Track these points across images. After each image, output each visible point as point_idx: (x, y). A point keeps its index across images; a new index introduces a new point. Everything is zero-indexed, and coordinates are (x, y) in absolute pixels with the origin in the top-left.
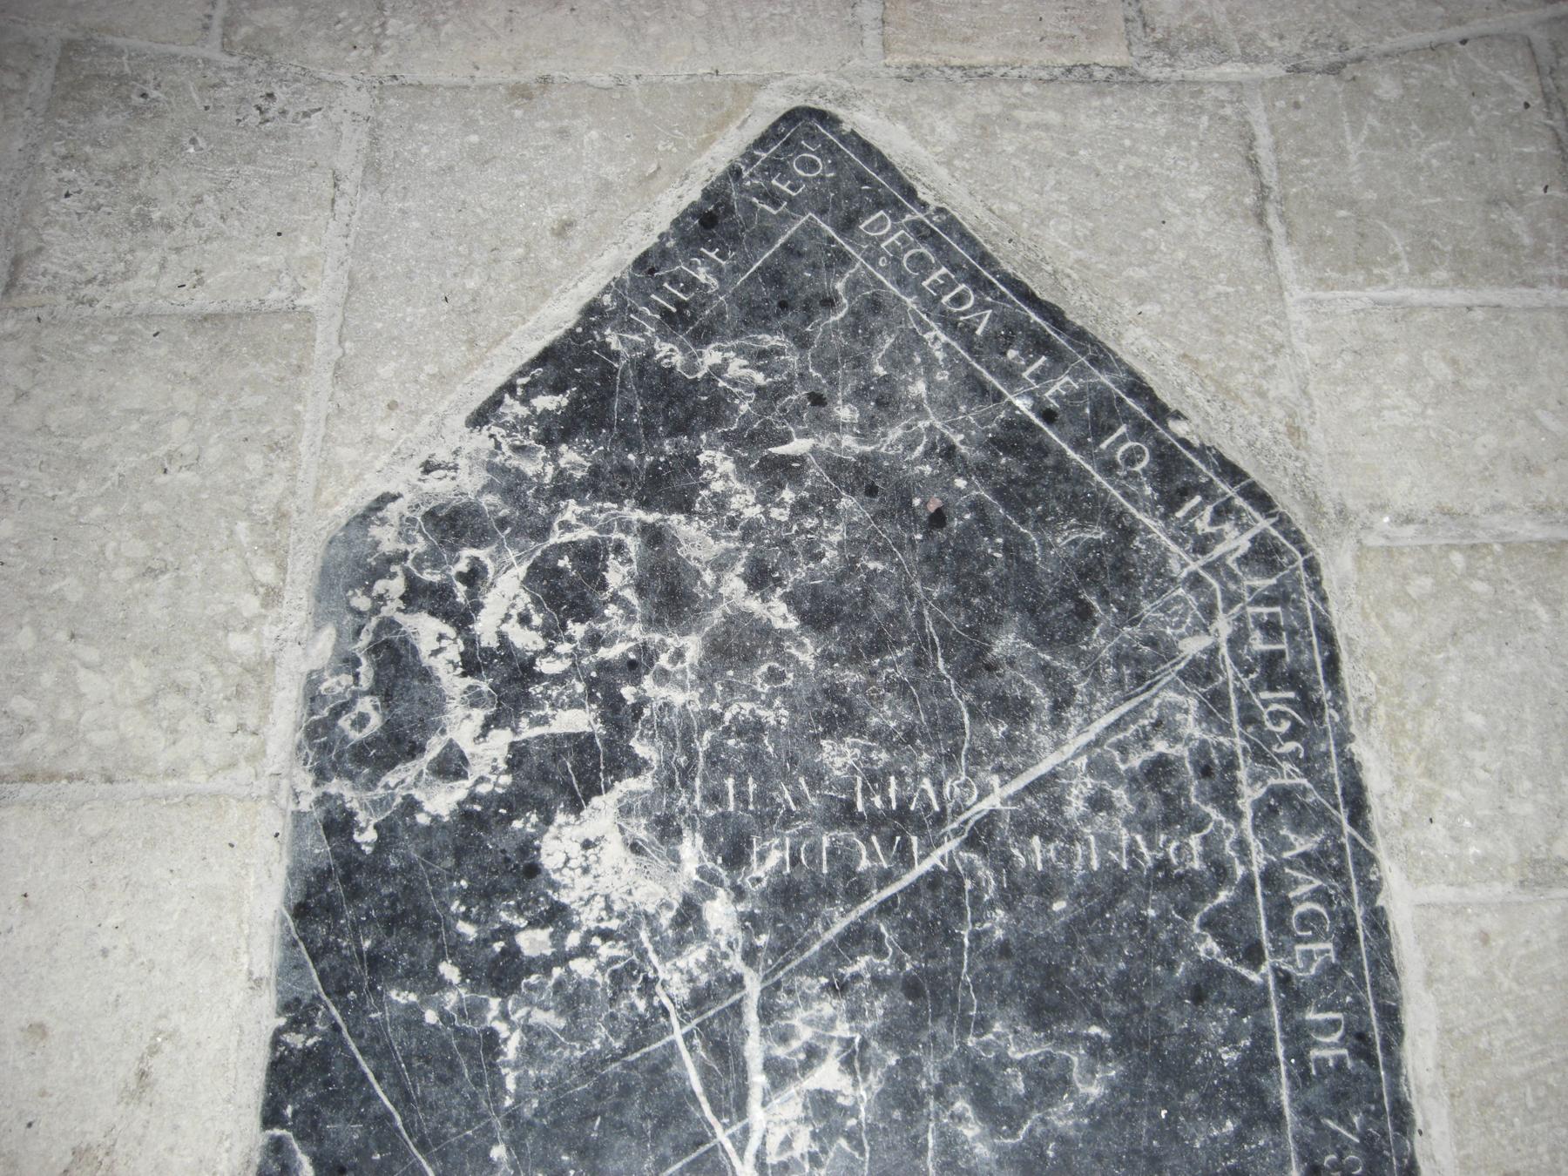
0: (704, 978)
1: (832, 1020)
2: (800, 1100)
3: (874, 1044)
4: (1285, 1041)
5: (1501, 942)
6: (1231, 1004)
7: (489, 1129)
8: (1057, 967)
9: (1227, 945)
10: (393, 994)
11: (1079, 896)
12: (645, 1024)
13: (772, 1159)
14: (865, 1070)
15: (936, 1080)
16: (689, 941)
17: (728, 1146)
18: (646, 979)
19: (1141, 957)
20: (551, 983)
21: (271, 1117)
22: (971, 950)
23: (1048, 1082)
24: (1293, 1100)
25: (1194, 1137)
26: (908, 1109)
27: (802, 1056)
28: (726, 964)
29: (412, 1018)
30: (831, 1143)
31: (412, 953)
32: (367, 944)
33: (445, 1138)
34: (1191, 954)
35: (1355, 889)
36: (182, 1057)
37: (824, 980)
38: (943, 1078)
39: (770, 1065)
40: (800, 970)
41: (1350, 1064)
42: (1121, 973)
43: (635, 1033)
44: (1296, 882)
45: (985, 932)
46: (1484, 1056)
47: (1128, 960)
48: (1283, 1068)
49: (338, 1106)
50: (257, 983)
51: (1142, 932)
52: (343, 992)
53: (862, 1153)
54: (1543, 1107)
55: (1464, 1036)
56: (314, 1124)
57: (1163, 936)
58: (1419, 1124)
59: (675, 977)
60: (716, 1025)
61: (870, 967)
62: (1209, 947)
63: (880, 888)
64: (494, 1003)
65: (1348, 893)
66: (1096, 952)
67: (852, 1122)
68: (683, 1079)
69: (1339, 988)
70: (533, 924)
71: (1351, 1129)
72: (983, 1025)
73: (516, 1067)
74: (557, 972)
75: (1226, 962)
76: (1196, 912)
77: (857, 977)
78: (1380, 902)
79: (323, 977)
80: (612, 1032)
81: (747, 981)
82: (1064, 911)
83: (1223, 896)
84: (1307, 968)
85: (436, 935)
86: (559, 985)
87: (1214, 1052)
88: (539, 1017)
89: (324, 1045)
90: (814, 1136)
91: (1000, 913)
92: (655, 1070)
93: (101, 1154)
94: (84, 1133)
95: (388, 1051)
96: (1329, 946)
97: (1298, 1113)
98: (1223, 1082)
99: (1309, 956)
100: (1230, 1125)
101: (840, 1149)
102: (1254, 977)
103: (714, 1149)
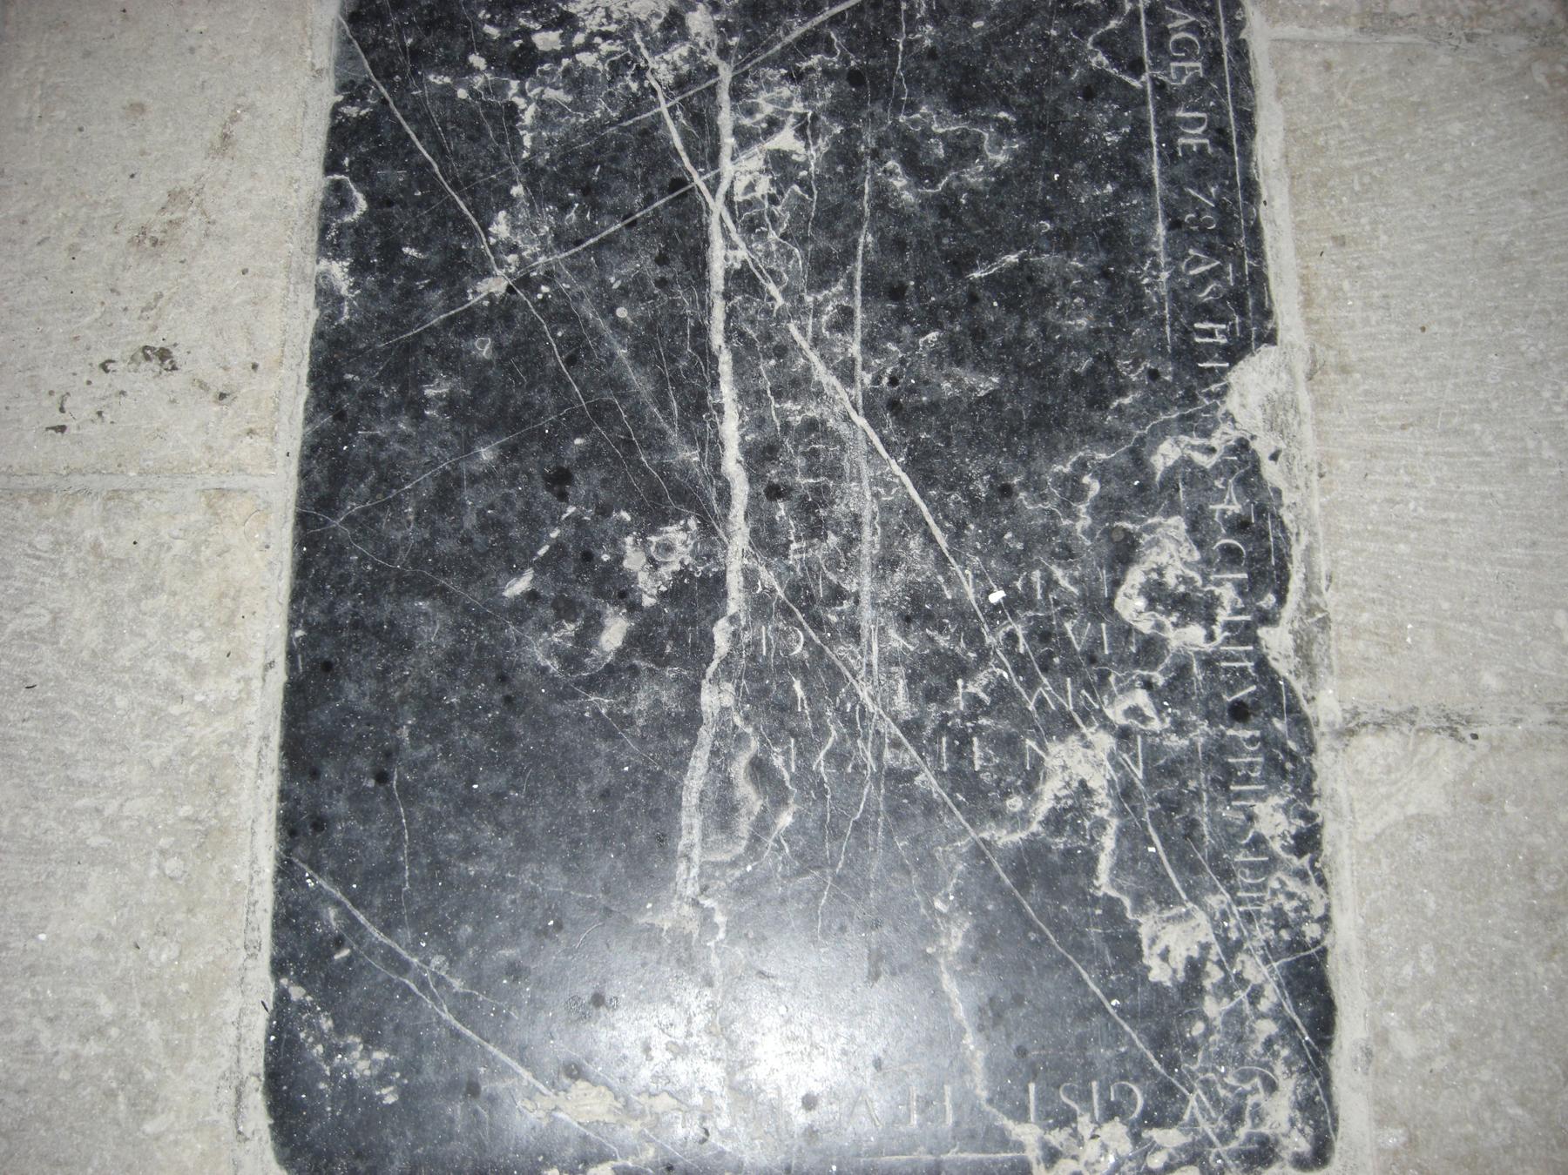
0: (686, 68)
1: (790, 100)
2: (762, 156)
3: (823, 118)
4: (1158, 131)
5: (1341, 70)
6: (1115, 101)
7: (509, 174)
8: (975, 69)
9: (1115, 59)
10: (431, 77)
11: (994, 18)
12: (636, 99)
13: (739, 198)
14: (815, 137)
15: (873, 145)
16: (674, 41)
17: (703, 188)
18: (638, 67)
19: (1043, 64)
20: (561, 70)
21: (332, 165)
22: (904, 53)
23: (963, 150)
24: (1161, 173)
25: (1080, 195)
26: (849, 165)
27: (764, 125)
28: (704, 58)
29: (447, 95)
30: (786, 187)
31: (446, 47)
32: (409, 41)
33: (474, 180)
34: (1085, 64)
35: (1222, 25)
36: (259, 123)
37: (784, 71)
38: (878, 143)
39: (738, 131)
40: (764, 63)
41: (1210, 150)
42: (1026, 74)
43: (628, 106)
44: (1174, 17)
45: (917, 41)
46: (1321, 151)
47: (1031, 65)
48: (1155, 150)
49: (386, 158)
50: (318, 73)
51: (1045, 46)
52: (389, 76)
53: (811, 195)
54: (1367, 191)
55: (1305, 135)
56: (367, 171)
57: (1062, 50)
58: (1265, 196)
59: (662, 68)
60: (695, 101)
61: (821, 63)
62: (1099, 59)
63: (831, 6)
64: (514, 84)
65: (1217, 27)
66: (1006, 58)
67: (804, 173)
68: (668, 139)
69: (1205, 95)
70: (546, 28)
71: (1209, 197)
72: (912, 107)
73: (532, 129)
74: (565, 62)
75: (1114, 71)
76: (1090, 33)
77: (811, 69)
78: (1243, 36)
79: (373, 65)
80: (610, 105)
81: (721, 71)
82: (982, 29)
83: (1113, 24)
84: (1179, 79)
85: (466, 34)
86: (567, 71)
87: (1100, 135)
88: (550, 94)
89: (375, 115)
90: (773, 182)
91: (929, 28)
92: (645, 133)
93: (192, 195)
94: (177, 181)
95: (427, 118)
96: (1199, 64)
97: (1166, 182)
98: (1106, 157)
99: (1181, 71)
100: (1109, 188)
101: (794, 193)
102: (1136, 84)
103: (692, 190)
